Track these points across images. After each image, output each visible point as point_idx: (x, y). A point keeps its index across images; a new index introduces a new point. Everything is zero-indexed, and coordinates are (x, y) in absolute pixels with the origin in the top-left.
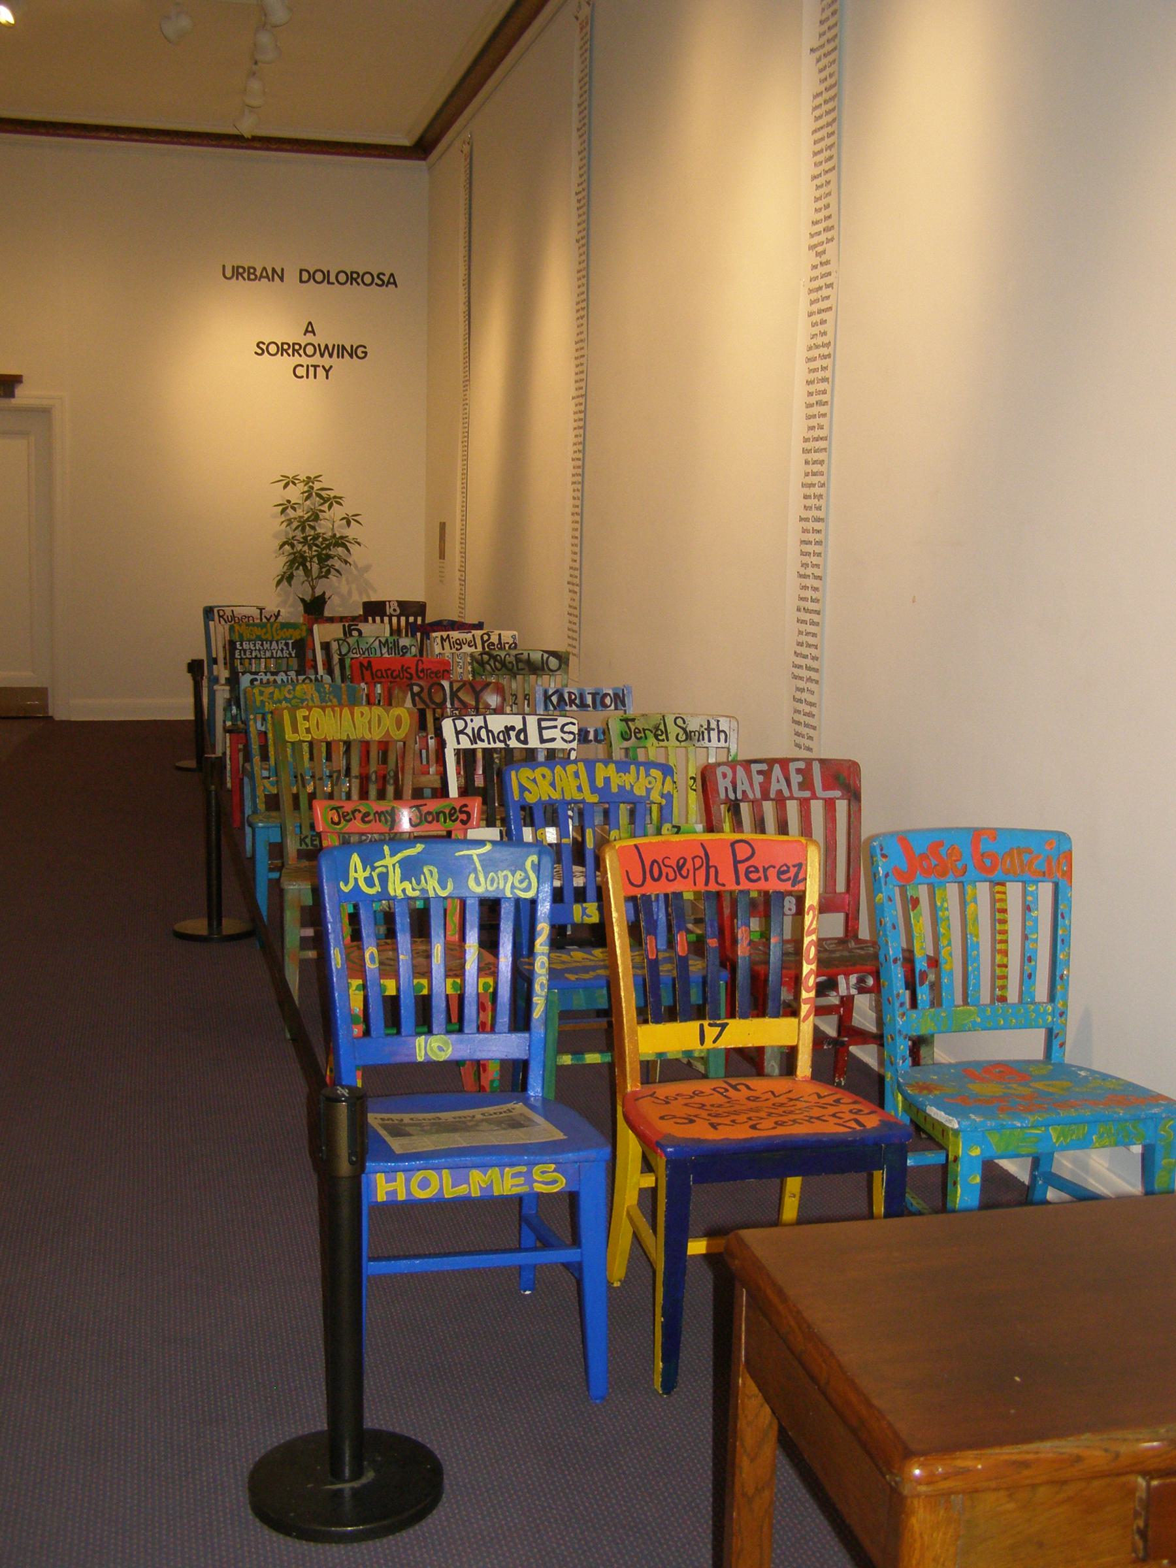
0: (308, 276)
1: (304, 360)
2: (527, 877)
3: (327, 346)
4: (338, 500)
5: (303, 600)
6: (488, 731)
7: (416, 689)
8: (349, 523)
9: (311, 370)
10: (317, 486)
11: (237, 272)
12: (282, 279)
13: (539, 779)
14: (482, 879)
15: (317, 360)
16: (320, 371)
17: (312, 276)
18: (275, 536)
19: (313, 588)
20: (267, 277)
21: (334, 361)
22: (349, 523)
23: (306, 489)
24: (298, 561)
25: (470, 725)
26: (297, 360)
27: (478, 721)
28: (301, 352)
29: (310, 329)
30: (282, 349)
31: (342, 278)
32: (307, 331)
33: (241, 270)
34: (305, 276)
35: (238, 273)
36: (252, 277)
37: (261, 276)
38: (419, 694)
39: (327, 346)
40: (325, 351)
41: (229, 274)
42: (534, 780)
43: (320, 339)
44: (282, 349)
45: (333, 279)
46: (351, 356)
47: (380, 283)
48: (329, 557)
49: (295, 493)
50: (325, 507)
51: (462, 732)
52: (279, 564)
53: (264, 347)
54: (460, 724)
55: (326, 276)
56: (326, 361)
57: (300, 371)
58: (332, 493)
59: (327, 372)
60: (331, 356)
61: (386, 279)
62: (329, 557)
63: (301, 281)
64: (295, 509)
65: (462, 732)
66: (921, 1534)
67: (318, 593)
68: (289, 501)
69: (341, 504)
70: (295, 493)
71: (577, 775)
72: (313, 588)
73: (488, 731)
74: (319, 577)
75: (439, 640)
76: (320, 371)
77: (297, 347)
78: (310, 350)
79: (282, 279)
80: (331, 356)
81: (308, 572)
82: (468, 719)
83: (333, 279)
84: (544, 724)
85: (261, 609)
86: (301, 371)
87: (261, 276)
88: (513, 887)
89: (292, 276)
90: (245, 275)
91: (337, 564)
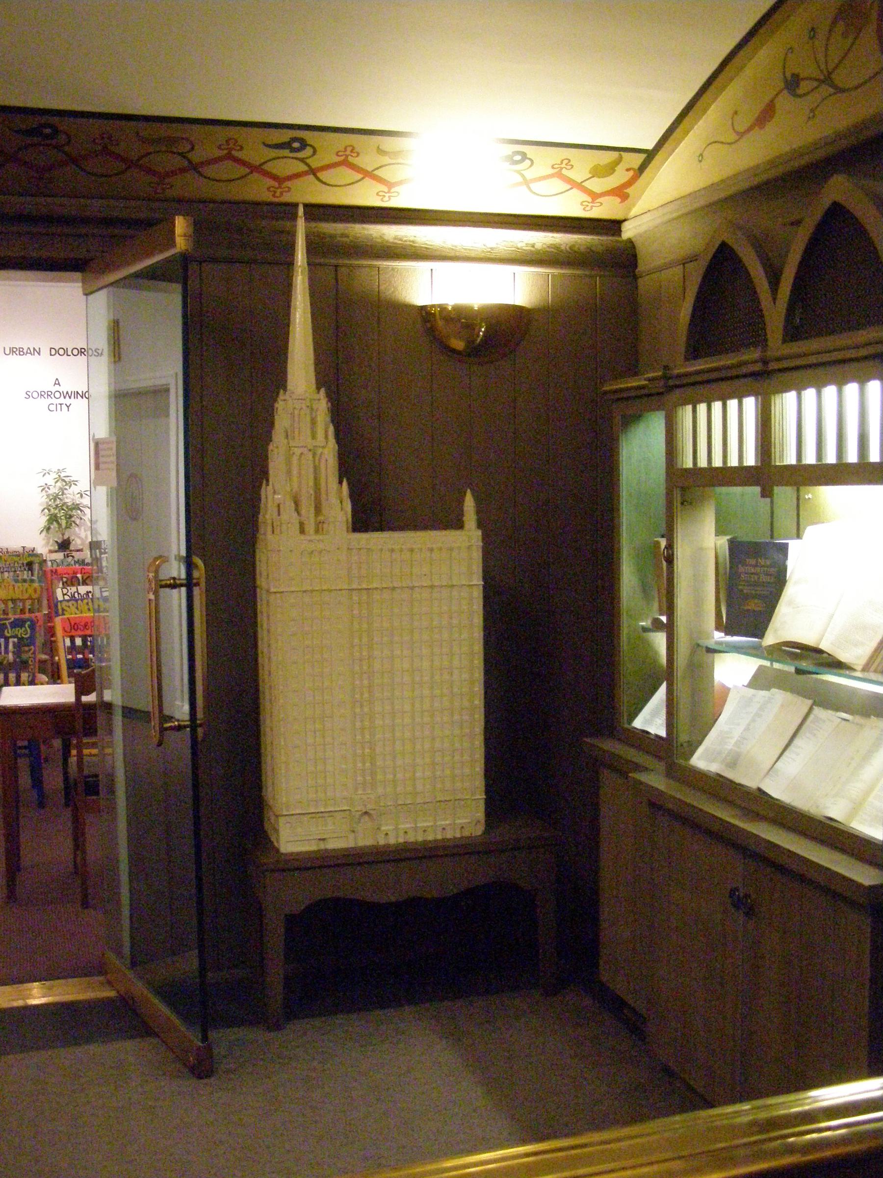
0: (55, 352)
1: (54, 401)
2: (26, 630)
3: (67, 393)
4: (75, 483)
5: (57, 542)
6: (79, 594)
7: (65, 580)
8: (82, 496)
9: (59, 406)
10: (63, 475)
11: (13, 351)
12: (39, 354)
13: (71, 605)
14: (10, 631)
15: (62, 400)
16: (64, 407)
17: (57, 352)
18: (41, 505)
19: (63, 535)
20: (31, 353)
21: (72, 401)
22: (82, 496)
23: (57, 476)
24: (53, 519)
25: (70, 591)
26: (50, 401)
27: (74, 589)
28: (52, 396)
29: (57, 383)
30: (41, 395)
31: (75, 352)
32: (55, 384)
33: (15, 350)
34: (53, 352)
35: (13, 351)
36: (21, 353)
37: (27, 353)
38: (66, 582)
39: (67, 393)
40: (67, 395)
41: (7, 352)
42: (69, 607)
43: (64, 388)
44: (41, 395)
45: (70, 353)
46: (82, 397)
47: (96, 354)
48: (71, 517)
49: (50, 480)
50: (67, 487)
51: (66, 594)
52: (43, 521)
53: (30, 394)
54: (65, 591)
55: (66, 351)
56: (67, 401)
57: (53, 407)
58: (72, 479)
59: (68, 407)
60: (70, 397)
61: (100, 352)
62: (71, 517)
63: (51, 355)
64: (49, 489)
65: (66, 594)
66: (76, 784)
67: (66, 537)
68: (46, 484)
69: (76, 485)
70: (50, 480)
71: (87, 604)
72: (63, 535)
73: (79, 594)
74: (67, 528)
75: (105, 559)
76: (64, 407)
77: (50, 393)
78: (57, 395)
79: (39, 354)
80: (70, 397)
81: (60, 525)
82: (69, 588)
83: (70, 353)
84: (103, 590)
85: (24, 547)
86: (53, 407)
87: (27, 353)
88: (21, 634)
89: (45, 352)
90: (17, 352)
91: (78, 521)
